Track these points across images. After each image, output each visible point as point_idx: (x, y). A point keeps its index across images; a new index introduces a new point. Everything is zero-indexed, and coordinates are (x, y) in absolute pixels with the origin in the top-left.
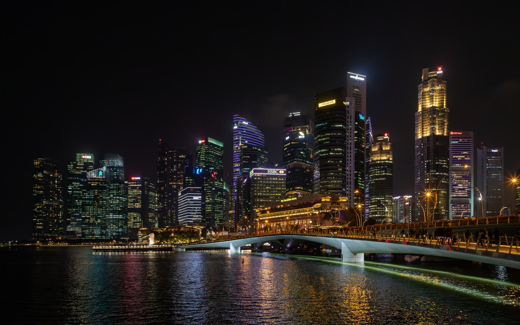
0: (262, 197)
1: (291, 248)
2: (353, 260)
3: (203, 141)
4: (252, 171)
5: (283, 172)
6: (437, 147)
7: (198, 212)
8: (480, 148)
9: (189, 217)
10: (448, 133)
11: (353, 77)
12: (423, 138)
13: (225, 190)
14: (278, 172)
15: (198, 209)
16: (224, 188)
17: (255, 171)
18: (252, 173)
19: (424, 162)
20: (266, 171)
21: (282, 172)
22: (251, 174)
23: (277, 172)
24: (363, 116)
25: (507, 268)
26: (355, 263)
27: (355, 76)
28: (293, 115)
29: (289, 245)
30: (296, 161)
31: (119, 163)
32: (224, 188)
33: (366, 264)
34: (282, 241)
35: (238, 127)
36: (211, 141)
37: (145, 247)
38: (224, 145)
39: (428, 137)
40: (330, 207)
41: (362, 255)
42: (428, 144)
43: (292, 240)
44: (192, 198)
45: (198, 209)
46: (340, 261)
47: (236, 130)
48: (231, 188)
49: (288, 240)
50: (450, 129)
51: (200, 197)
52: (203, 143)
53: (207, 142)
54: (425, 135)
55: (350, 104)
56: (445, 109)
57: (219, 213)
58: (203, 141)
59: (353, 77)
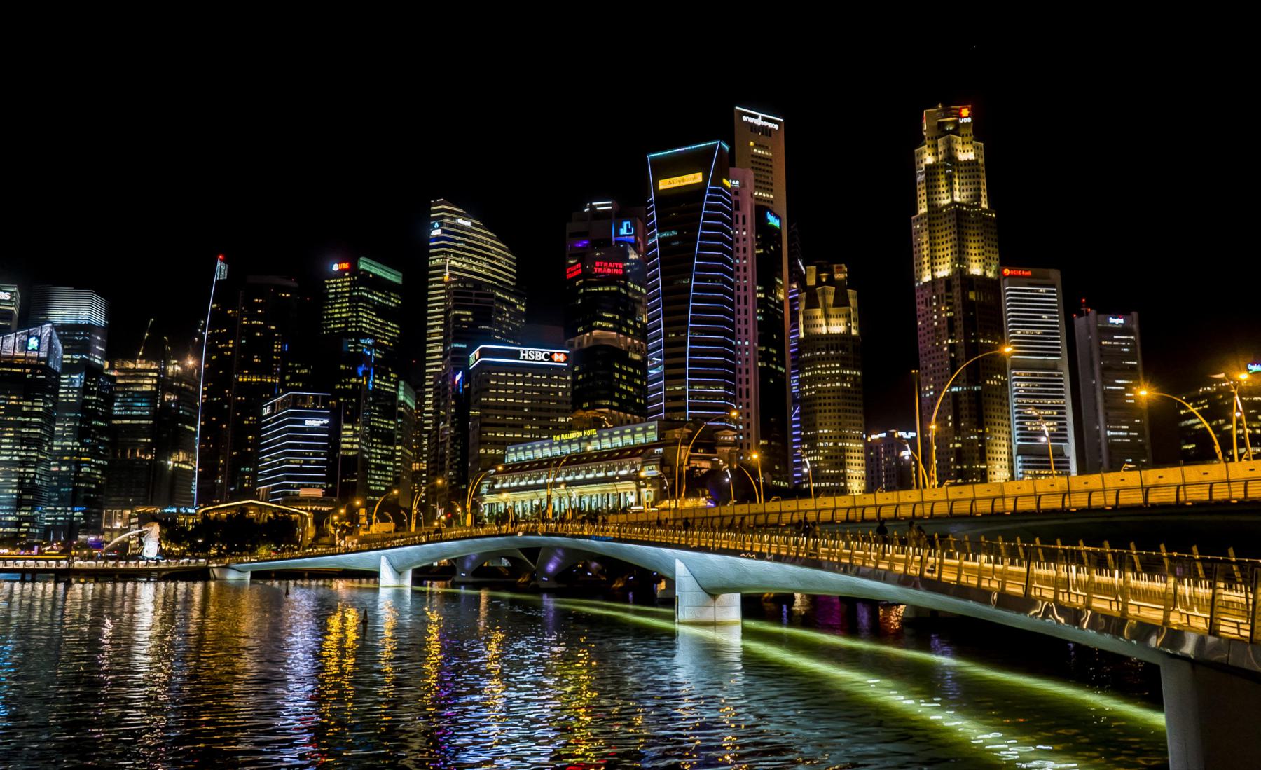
0: (503, 426)
1: (559, 576)
2: (708, 615)
3: (345, 266)
4: (477, 352)
5: (562, 358)
6: (979, 310)
7: (317, 463)
8: (1080, 314)
9: (289, 478)
10: (998, 272)
11: (751, 120)
12: (934, 281)
13: (403, 403)
14: (549, 357)
15: (316, 455)
16: (401, 398)
17: (484, 353)
18: (474, 358)
19: (941, 343)
20: (516, 355)
21: (560, 357)
22: (472, 360)
23: (546, 356)
24: (777, 217)
25: (809, 596)
26: (714, 624)
27: (756, 117)
28: (593, 208)
29: (551, 567)
30: (600, 328)
31: (93, 313)
32: (401, 398)
33: (747, 634)
34: (533, 552)
35: (444, 231)
36: (363, 265)
37: (132, 564)
38: (404, 279)
39: (947, 281)
40: (690, 458)
41: (737, 598)
42: (948, 297)
43: (560, 553)
44: (303, 422)
45: (316, 455)
46: (671, 618)
47: (438, 238)
48: (420, 399)
49: (552, 549)
50: (1004, 263)
51: (326, 421)
52: (342, 272)
53: (354, 270)
54: (939, 274)
55: (743, 185)
56: (984, 210)
57: (383, 468)
58: (345, 266)
59: (751, 120)
